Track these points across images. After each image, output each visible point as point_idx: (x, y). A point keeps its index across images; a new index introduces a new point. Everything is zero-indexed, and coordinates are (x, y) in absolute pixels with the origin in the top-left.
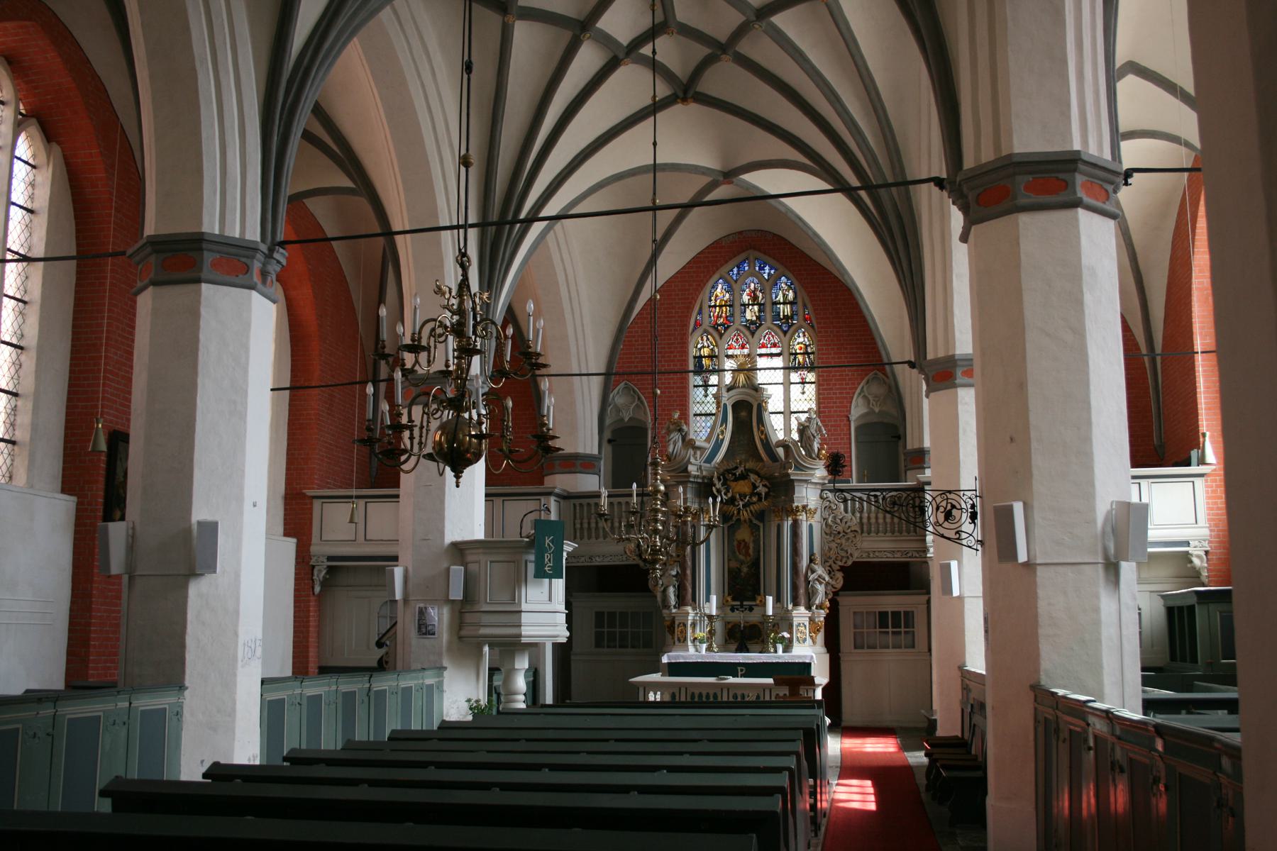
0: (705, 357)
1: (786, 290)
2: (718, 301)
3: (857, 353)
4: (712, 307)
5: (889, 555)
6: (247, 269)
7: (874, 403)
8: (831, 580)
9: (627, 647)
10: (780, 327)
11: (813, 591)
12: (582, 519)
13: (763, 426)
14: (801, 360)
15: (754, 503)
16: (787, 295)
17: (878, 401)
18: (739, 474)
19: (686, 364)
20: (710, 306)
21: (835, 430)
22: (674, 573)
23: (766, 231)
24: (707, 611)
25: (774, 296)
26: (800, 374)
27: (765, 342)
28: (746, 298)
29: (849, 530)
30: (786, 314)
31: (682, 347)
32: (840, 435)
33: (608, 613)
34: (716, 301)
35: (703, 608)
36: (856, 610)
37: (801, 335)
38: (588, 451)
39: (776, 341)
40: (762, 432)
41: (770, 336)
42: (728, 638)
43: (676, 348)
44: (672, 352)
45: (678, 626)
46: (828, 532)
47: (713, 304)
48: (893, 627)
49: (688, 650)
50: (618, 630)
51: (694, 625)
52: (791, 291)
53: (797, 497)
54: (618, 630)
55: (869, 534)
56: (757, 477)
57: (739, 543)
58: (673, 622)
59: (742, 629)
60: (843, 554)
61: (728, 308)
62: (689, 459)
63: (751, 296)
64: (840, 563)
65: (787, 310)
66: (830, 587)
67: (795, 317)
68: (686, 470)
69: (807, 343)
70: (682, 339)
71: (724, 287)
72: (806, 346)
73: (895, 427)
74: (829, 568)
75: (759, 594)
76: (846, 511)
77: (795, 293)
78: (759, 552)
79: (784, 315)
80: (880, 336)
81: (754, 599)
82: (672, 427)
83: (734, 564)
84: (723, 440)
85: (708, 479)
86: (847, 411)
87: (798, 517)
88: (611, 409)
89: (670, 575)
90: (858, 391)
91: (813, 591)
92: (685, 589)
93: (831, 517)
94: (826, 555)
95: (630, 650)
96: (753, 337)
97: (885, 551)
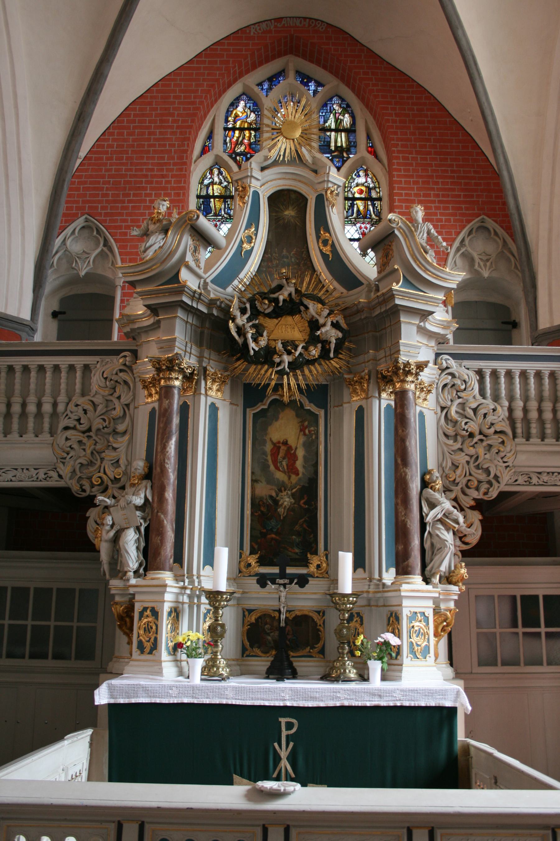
0: (214, 197)
1: (340, 114)
3: (454, 190)
4: (229, 129)
7: (482, 264)
9: (44, 656)
11: (432, 545)
13: (327, 230)
14: (361, 208)
15: (312, 362)
16: (342, 121)
17: (488, 260)
18: (284, 301)
19: (184, 194)
20: (226, 129)
22: (139, 501)
23: (316, 20)
24: (208, 585)
25: (322, 120)
26: (361, 228)
29: (492, 430)
30: (339, 144)
31: (181, 170)
34: (235, 122)
35: (199, 577)
36: (481, 592)
37: (361, 173)
38: (12, 311)
42: (247, 644)
43: (172, 170)
44: (163, 176)
45: (141, 614)
46: (451, 431)
47: (230, 126)
48: (547, 626)
49: (160, 672)
50: (30, 623)
51: (176, 613)
52: (347, 115)
53: (406, 345)
56: (320, 306)
57: (276, 447)
58: (130, 608)
59: (283, 624)
60: (483, 477)
61: (253, 133)
62: (184, 255)
64: (475, 494)
65: (342, 139)
67: (353, 150)
68: (176, 278)
70: (181, 158)
72: (369, 189)
76: (482, 393)
77: (353, 117)
78: (316, 465)
79: (336, 146)
81: (305, 563)
82: (152, 227)
83: (264, 490)
85: (220, 308)
88: (59, 259)
89: (129, 503)
92: (161, 533)
94: (447, 477)
95: (50, 663)
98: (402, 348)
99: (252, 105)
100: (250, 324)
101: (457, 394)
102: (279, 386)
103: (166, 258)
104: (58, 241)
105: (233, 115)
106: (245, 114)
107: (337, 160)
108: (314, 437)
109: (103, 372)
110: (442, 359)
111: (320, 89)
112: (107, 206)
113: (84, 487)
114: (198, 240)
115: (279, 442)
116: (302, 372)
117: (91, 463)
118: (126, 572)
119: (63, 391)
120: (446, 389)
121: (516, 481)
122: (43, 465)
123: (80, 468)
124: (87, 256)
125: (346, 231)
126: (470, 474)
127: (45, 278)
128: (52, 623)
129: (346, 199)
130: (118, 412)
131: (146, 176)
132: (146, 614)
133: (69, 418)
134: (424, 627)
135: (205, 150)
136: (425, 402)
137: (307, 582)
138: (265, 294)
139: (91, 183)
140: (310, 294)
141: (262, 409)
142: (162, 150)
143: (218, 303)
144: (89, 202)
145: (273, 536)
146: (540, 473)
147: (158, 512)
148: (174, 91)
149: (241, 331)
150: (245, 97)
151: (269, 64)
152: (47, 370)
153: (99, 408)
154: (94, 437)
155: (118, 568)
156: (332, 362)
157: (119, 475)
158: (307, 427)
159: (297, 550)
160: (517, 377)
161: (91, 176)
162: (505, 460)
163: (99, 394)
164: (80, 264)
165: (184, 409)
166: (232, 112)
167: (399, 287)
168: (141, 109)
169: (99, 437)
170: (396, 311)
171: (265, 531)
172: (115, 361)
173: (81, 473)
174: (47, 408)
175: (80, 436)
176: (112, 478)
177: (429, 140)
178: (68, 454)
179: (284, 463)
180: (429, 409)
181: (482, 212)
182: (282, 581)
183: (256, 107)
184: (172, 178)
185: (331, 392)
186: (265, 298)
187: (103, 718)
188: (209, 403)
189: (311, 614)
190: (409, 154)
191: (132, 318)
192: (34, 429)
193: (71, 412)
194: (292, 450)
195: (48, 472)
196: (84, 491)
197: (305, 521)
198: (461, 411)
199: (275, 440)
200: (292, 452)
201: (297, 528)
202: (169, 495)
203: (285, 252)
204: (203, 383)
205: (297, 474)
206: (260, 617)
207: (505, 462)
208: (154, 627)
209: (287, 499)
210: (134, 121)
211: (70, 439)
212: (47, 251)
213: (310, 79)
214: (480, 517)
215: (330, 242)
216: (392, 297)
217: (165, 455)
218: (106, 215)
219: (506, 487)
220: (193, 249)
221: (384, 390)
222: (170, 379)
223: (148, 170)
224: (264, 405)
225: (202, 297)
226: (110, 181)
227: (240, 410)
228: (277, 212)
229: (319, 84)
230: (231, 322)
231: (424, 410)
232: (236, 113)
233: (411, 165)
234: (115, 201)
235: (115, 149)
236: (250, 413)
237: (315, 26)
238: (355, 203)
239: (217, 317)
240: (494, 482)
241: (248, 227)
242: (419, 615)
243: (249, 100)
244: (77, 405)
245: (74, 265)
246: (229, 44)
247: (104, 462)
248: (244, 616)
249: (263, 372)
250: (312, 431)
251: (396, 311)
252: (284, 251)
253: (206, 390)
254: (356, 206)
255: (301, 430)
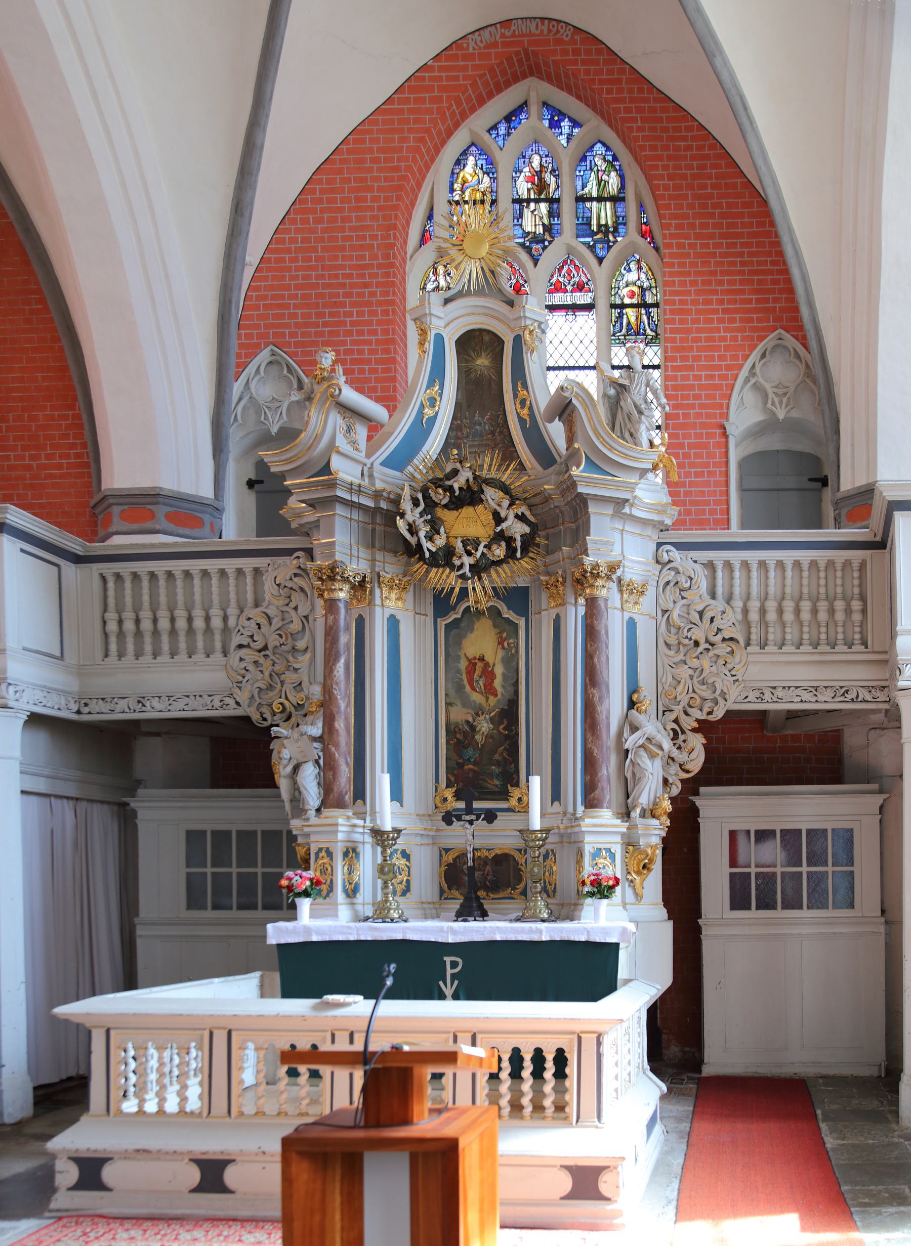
2: (467, 193)
3: (742, 292)
5: (806, 696)
6: (152, 516)
7: (776, 400)
8: (674, 749)
10: (592, 248)
11: (634, 774)
12: (119, 611)
13: (525, 386)
14: (633, 319)
15: (499, 563)
16: (606, 182)
17: (785, 394)
21: (697, 456)
25: (579, 183)
27: (561, 280)
28: (523, 188)
29: (719, 637)
30: (603, 222)
32: (707, 465)
33: (215, 833)
37: (633, 266)
38: (187, 487)
39: (585, 280)
40: (523, 403)
41: (572, 268)
44: (365, 285)
48: (809, 864)
52: (613, 174)
54: (234, 870)
55: (762, 648)
60: (707, 694)
63: (533, 183)
66: (674, 768)
67: (622, 229)
68: (326, 469)
69: (646, 285)
71: (479, 163)
72: (643, 290)
73: (816, 461)
74: (675, 726)
75: (517, 784)
77: (622, 177)
79: (599, 226)
80: (790, 230)
83: (460, 715)
84: (433, 420)
85: (389, 500)
86: (722, 396)
87: (597, 593)
88: (244, 408)
90: (744, 373)
91: (634, 774)
93: (679, 605)
96: (536, 265)
97: (797, 687)
98: (589, 546)
99: (484, 162)
100: (422, 519)
101: (680, 594)
102: (464, 593)
103: (312, 444)
104: (237, 387)
105: (460, 180)
106: (476, 177)
107: (601, 246)
108: (513, 651)
109: (276, 577)
110: (663, 551)
111: (576, 130)
112: (297, 332)
113: (264, 716)
114: (351, 417)
115: (475, 658)
116: (489, 576)
117: (271, 687)
118: (306, 811)
119: (233, 603)
120: (668, 587)
121: (747, 697)
122: (217, 691)
123: (259, 692)
124: (278, 404)
125: (613, 355)
126: (694, 691)
127: (227, 440)
128: (259, 870)
129: (613, 306)
130: (296, 626)
131: (343, 285)
132: (321, 855)
133: (242, 634)
134: (609, 864)
135: (424, 239)
136: (637, 606)
137: (495, 817)
138: (441, 480)
139: (273, 297)
140: (492, 479)
141: (455, 619)
142: (361, 245)
143: (384, 494)
144: (273, 326)
145: (471, 766)
146: (774, 688)
147: (328, 744)
148: (371, 150)
149: (412, 530)
150: (475, 149)
151: (518, 84)
152: (212, 575)
153: (274, 621)
154: (272, 657)
155: (301, 807)
156: (522, 562)
157: (302, 700)
158: (505, 639)
159: (497, 782)
160: (755, 570)
161: (272, 288)
162: (733, 673)
163: (273, 604)
164: (270, 416)
165: (360, 622)
166: (458, 174)
167: (581, 472)
168: (329, 182)
169: (277, 656)
170: (583, 500)
171: (461, 761)
172: (288, 562)
173: (260, 698)
174: (216, 622)
175: (255, 655)
176: (296, 704)
177: (712, 216)
178: (244, 677)
179: (481, 683)
180: (642, 614)
181: (778, 324)
182: (468, 818)
183: (490, 168)
184: (377, 287)
185: (532, 597)
186: (440, 486)
187: (275, 955)
188: (387, 615)
189: (512, 853)
190: (686, 239)
191: (298, 511)
192: (204, 648)
193: (244, 627)
194: (489, 667)
195: (224, 699)
196: (265, 719)
197: (505, 749)
198: (686, 615)
199: (470, 656)
200: (490, 669)
201: (497, 757)
202: (340, 725)
203: (477, 417)
204: (377, 591)
205: (496, 695)
206: (458, 857)
207: (733, 676)
208: (329, 869)
209: (485, 725)
210: (320, 201)
211: (244, 660)
212: (223, 402)
213: (562, 115)
214: (704, 741)
215: (528, 403)
216: (574, 485)
217: (333, 679)
218: (297, 345)
219: (734, 704)
220: (345, 428)
221: (580, 595)
222: (332, 590)
223: (346, 276)
224: (456, 613)
225: (362, 489)
226: (297, 294)
227: (430, 620)
228: (467, 361)
229: (575, 124)
230: (398, 518)
231: (635, 616)
232: (464, 176)
233: (687, 255)
234: (306, 325)
235: (300, 245)
236: (442, 623)
237: (558, 32)
238: (624, 311)
239: (387, 510)
240: (720, 699)
241: (430, 385)
242: (604, 852)
243: (480, 154)
244: (249, 619)
245: (262, 418)
246: (441, 69)
247: (285, 686)
248: (441, 856)
249: (444, 577)
250: (512, 643)
251: (583, 500)
252: (477, 415)
253: (382, 600)
254: (625, 316)
255: (499, 644)
